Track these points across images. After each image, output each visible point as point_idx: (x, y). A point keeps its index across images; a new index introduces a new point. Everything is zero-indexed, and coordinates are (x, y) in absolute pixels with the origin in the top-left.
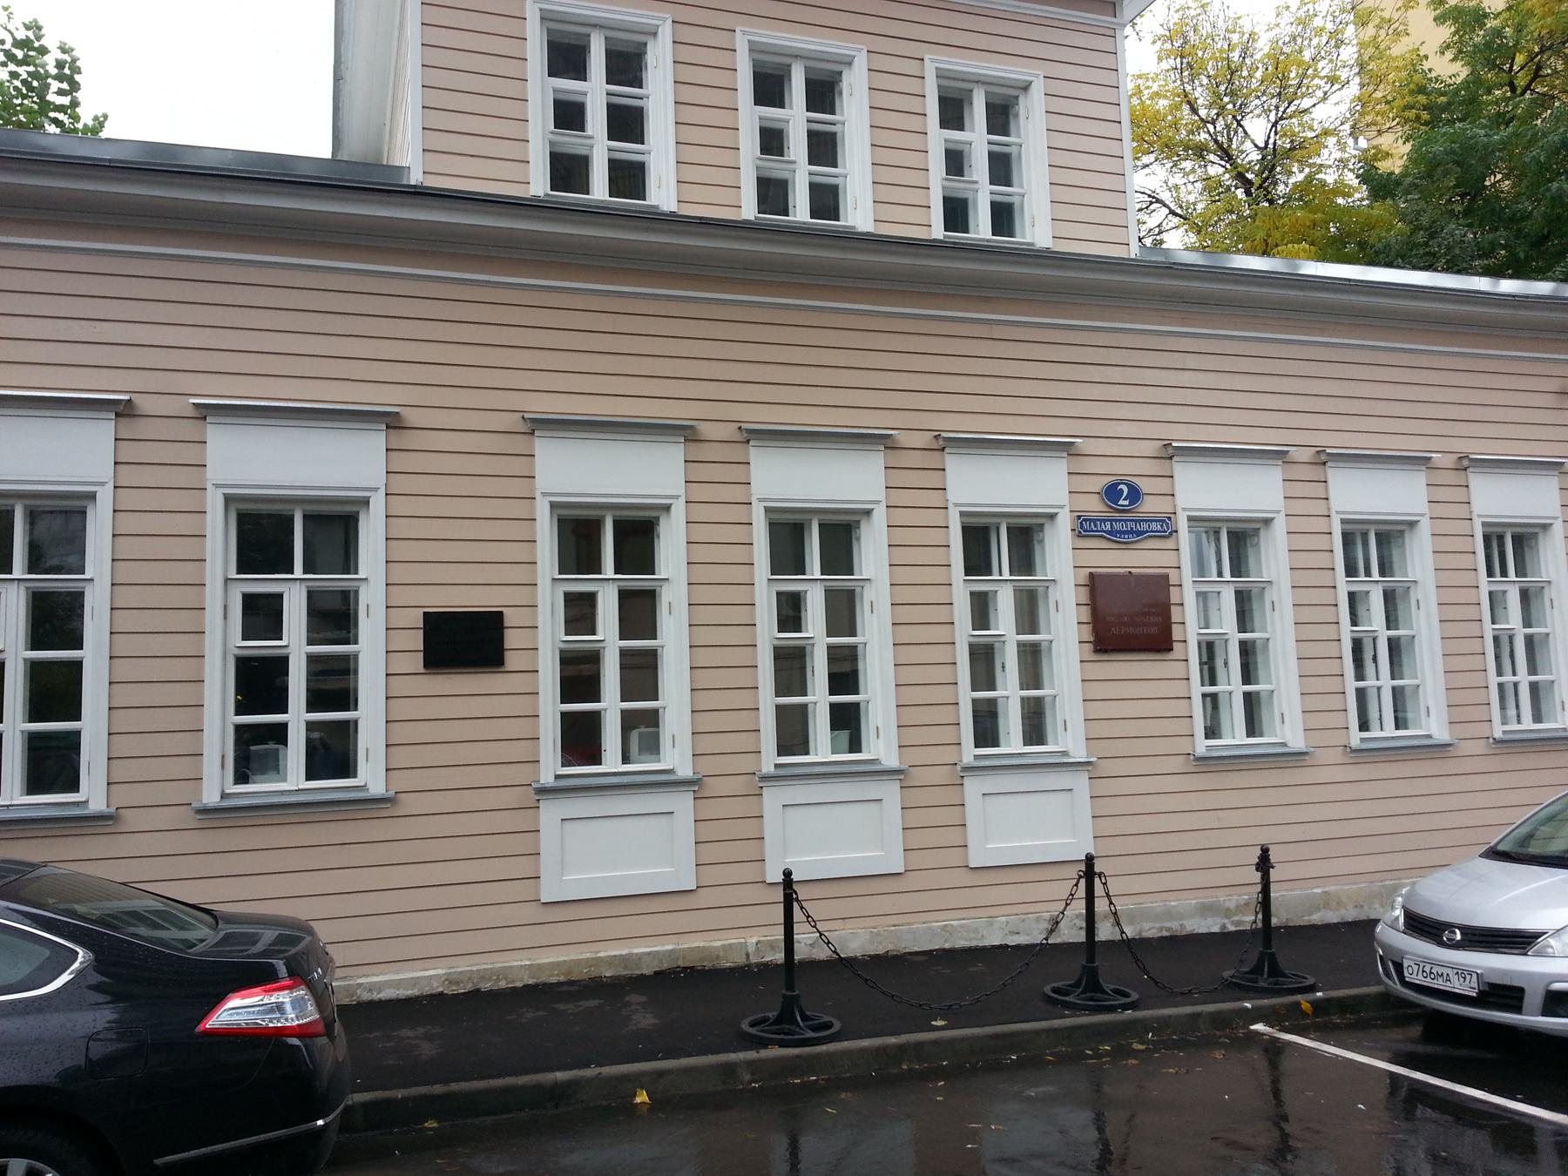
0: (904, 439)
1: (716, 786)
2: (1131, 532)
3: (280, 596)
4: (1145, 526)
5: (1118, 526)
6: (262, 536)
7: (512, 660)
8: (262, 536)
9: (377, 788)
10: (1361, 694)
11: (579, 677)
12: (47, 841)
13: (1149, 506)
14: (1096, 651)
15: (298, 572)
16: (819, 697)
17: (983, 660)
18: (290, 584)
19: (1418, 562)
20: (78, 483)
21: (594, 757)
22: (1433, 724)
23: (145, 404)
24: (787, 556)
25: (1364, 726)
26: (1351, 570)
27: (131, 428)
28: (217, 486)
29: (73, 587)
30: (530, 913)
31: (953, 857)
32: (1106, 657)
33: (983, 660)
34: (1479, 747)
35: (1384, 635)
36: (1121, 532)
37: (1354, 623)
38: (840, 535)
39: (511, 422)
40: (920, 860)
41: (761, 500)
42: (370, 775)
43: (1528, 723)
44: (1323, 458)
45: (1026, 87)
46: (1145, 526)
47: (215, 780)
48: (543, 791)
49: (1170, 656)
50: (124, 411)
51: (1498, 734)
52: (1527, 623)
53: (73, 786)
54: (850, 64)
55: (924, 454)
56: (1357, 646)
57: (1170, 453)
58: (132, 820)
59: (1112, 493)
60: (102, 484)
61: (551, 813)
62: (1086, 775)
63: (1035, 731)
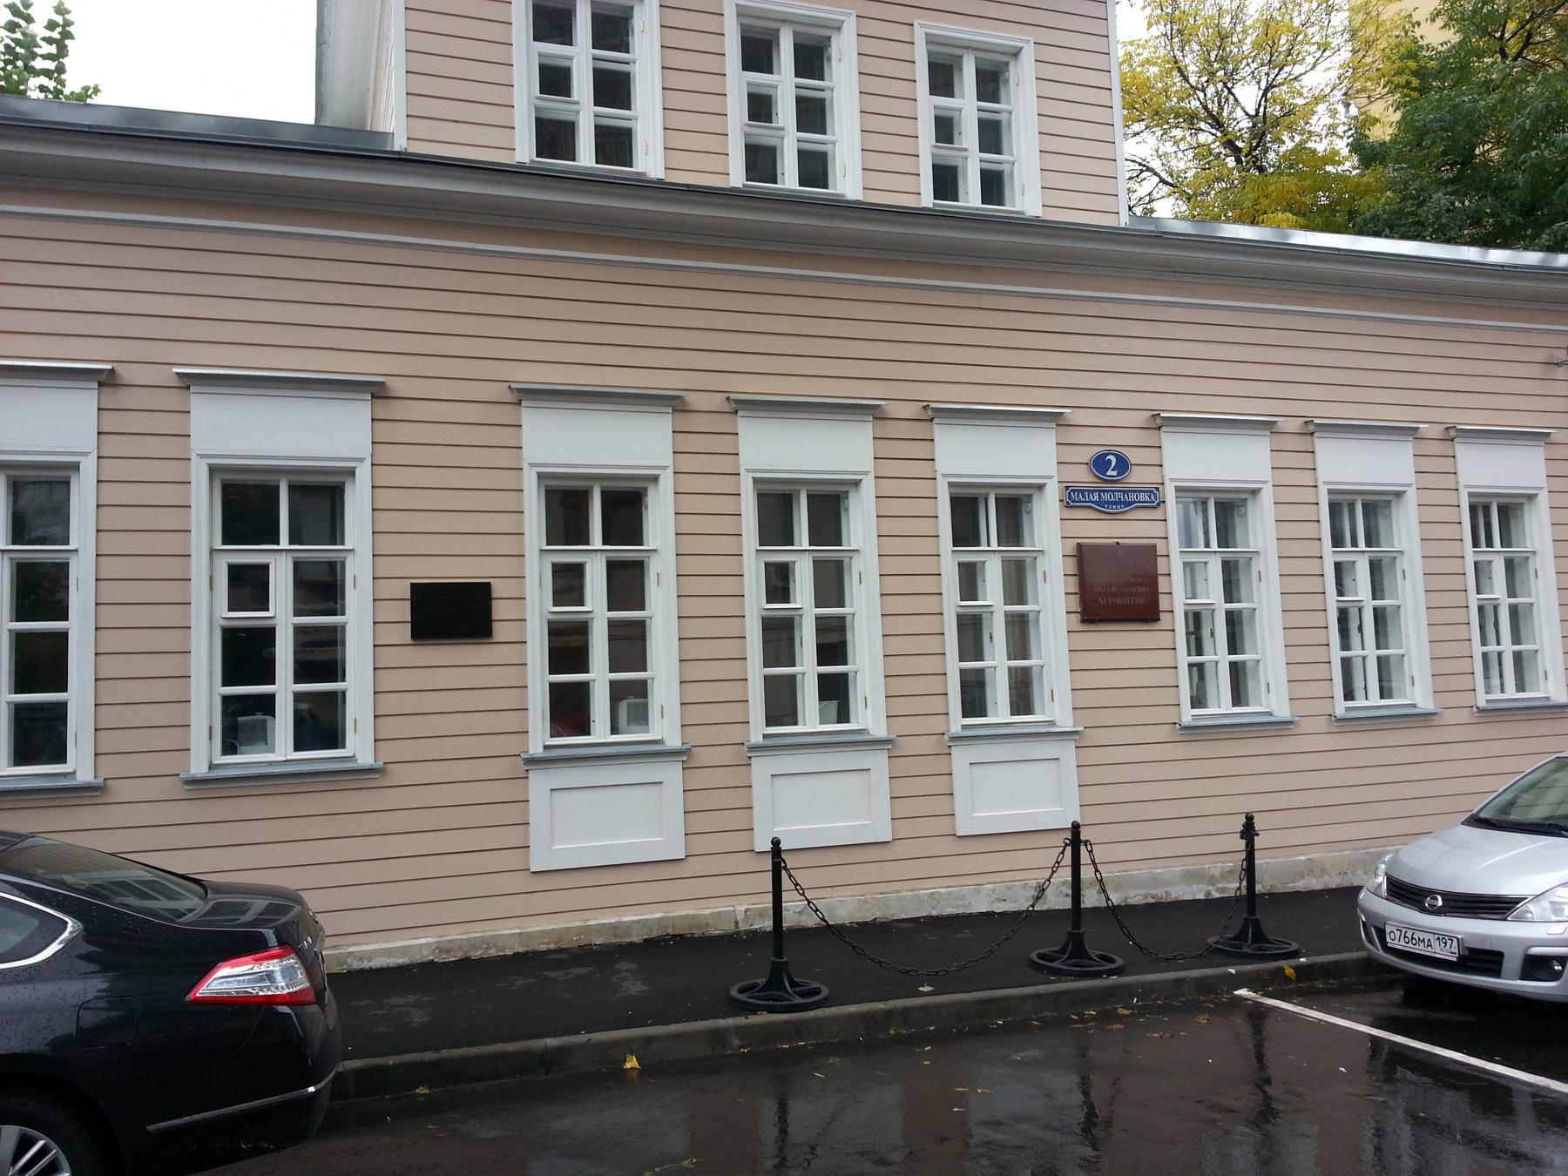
0: (893, 409)
1: (703, 757)
2: (1119, 502)
3: (266, 568)
4: (1133, 497)
5: (1106, 497)
6: (247, 506)
7: (500, 631)
8: (247, 506)
9: (366, 759)
10: (1346, 664)
11: (567, 647)
12: (18, 812)
13: (1137, 477)
14: (1084, 621)
15: (284, 543)
16: (807, 668)
17: (971, 630)
18: (277, 556)
19: (1405, 533)
20: (303, 458)
21: (583, 728)
22: (1417, 693)
23: (127, 373)
24: (776, 527)
25: (1349, 695)
26: (1337, 541)
27: (114, 398)
28: (202, 456)
29: (58, 558)
30: (950, 846)
31: (940, 826)
32: (1093, 627)
33: (971, 630)
34: (1463, 716)
35: (1369, 605)
36: (1109, 503)
37: (1340, 593)
38: (829, 506)
39: (498, 392)
40: (908, 829)
41: (749, 471)
42: (359, 746)
43: (1511, 692)
44: (1311, 429)
45: (1016, 54)
46: (1133, 497)
47: (203, 752)
48: (532, 761)
49: (1157, 626)
50: (106, 380)
51: (1482, 703)
52: (1512, 592)
53: (61, 757)
54: (839, 29)
55: (909, 425)
56: (1343, 616)
57: (1159, 423)
58: (122, 790)
59: (1100, 463)
60: (86, 454)
61: (539, 783)
62: (885, 755)
63: (1022, 700)
